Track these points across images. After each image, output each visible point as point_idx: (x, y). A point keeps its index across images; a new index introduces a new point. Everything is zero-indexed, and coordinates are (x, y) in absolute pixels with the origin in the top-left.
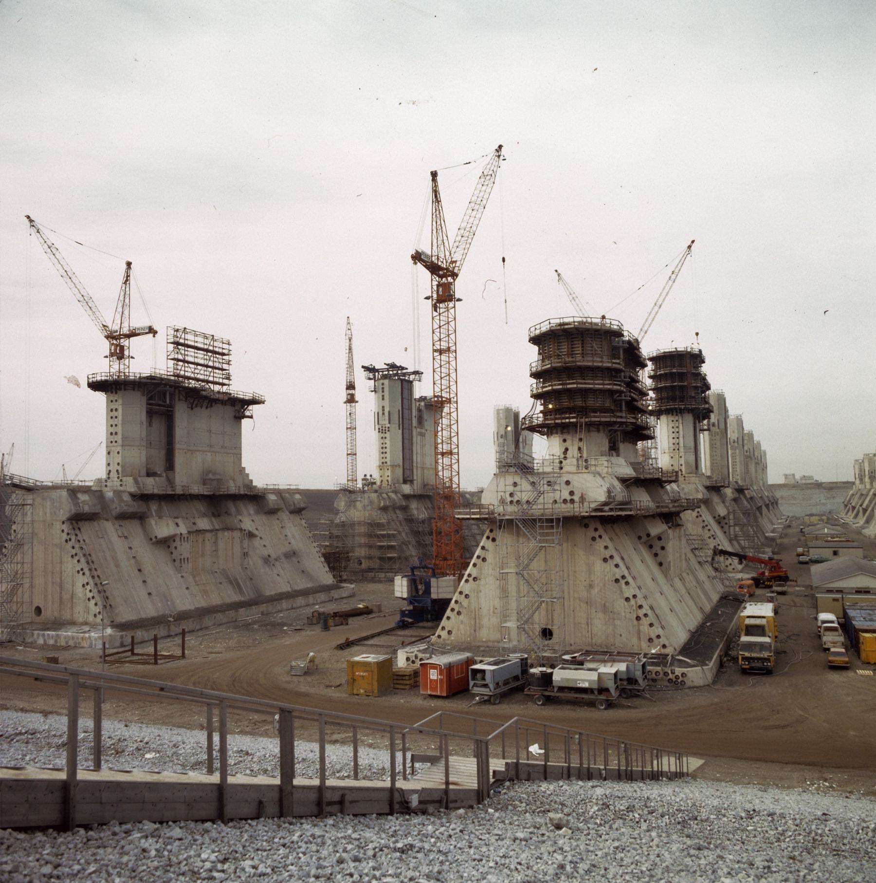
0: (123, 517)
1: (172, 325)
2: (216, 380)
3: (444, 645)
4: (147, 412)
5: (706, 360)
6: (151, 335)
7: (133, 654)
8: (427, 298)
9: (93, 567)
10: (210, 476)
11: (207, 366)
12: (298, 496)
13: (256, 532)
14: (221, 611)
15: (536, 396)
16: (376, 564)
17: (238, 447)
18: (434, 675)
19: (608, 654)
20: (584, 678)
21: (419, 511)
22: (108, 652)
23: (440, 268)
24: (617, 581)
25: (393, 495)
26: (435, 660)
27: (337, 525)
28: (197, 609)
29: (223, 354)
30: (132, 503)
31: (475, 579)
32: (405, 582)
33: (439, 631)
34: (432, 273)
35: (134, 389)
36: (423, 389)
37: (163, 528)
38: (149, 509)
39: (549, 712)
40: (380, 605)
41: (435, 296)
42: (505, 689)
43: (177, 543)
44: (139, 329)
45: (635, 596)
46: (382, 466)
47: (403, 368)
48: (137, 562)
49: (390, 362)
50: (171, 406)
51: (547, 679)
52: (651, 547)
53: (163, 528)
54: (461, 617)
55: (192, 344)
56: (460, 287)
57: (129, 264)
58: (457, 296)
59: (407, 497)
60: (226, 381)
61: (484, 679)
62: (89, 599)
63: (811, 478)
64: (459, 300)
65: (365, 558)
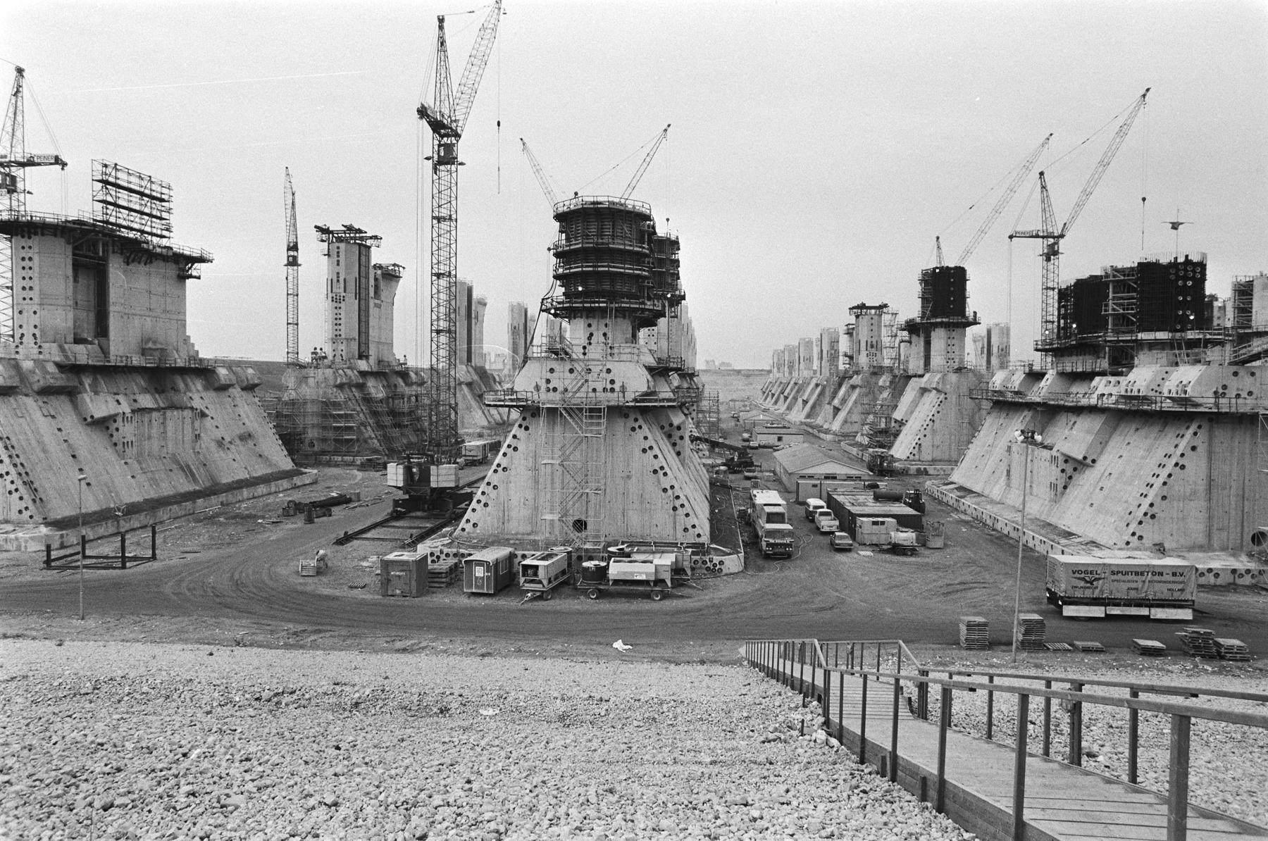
0: (47, 392)
1: (99, 157)
2: (154, 231)
3: (469, 539)
4: (73, 265)
5: (917, 275)
6: (59, 167)
7: (85, 557)
8: (428, 159)
9: (14, 453)
10: (150, 345)
11: (142, 213)
12: (250, 371)
13: (207, 411)
14: (176, 503)
15: (556, 277)
16: (330, 447)
17: (182, 312)
18: (479, 572)
19: (662, 546)
20: (639, 569)
21: (376, 390)
22: (54, 554)
23: (444, 126)
24: (655, 472)
25: (349, 372)
26: (477, 556)
27: (286, 403)
28: (146, 501)
29: (163, 200)
30: (59, 375)
31: (505, 469)
32: (401, 470)
33: (462, 524)
34: (434, 131)
35: (55, 236)
36: (378, 256)
37: (100, 406)
38: (81, 383)
39: (606, 605)
40: (358, 494)
41: (436, 156)
42: (555, 583)
43: (119, 423)
44: (39, 157)
45: (672, 487)
46: (336, 339)
47: (360, 231)
48: (70, 446)
49: (347, 224)
50: (105, 259)
51: (602, 572)
52: (669, 436)
53: (100, 406)
54: (488, 509)
55: (125, 184)
56: (463, 150)
57: (20, 71)
58: (460, 160)
59: (363, 374)
60: (165, 233)
61: (536, 574)
62: (10, 492)
63: (728, 365)
64: (462, 164)
65: (318, 439)
